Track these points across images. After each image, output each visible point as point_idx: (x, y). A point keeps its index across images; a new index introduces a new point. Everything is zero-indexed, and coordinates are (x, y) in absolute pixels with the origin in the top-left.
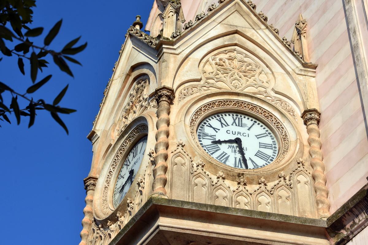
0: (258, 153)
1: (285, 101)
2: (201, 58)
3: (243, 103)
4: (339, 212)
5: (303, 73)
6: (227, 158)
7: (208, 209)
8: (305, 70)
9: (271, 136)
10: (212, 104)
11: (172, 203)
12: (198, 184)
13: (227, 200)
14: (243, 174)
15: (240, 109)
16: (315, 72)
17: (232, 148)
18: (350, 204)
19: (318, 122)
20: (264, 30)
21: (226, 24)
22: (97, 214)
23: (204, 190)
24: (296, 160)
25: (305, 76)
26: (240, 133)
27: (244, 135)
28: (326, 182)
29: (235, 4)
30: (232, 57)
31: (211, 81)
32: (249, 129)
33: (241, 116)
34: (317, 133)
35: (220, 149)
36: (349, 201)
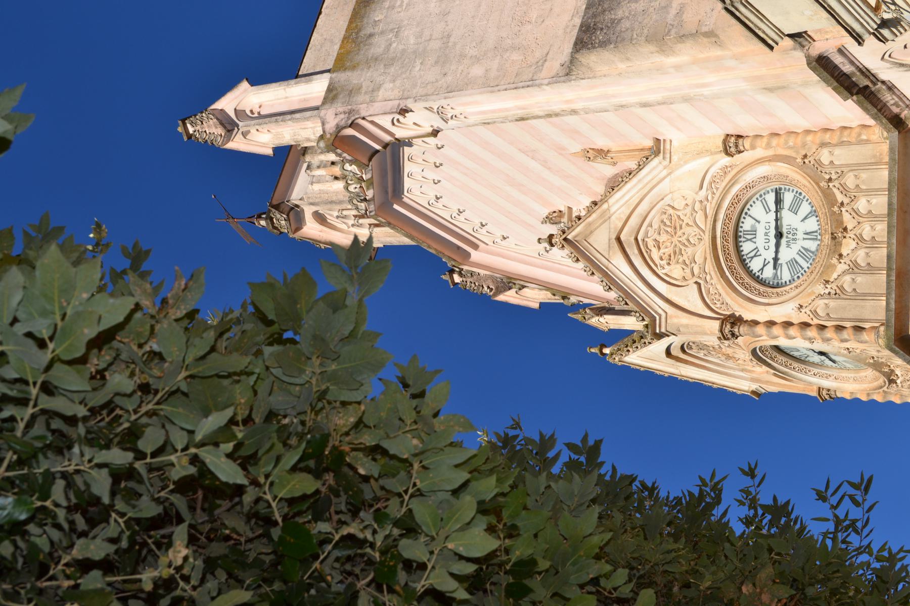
2: (665, 284)
4: (881, 122)
5: (668, 156)
6: (806, 250)
8: (664, 153)
9: (764, 194)
14: (832, 234)
15: (731, 233)
19: (739, 137)
27: (768, 227)
31: (696, 271)
32: (759, 222)
33: (741, 232)
36: (868, 114)
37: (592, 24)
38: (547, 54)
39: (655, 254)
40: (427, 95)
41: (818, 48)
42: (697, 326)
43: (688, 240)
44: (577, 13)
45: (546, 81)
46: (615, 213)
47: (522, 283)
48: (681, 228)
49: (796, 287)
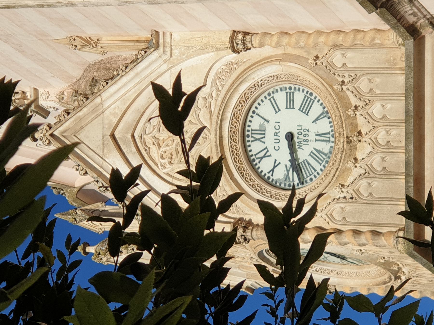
0: (304, 111)
1: (217, 73)
3: (231, 131)
4: (399, 31)
5: (168, 49)
7: (411, 185)
9: (273, 93)
10: (240, 172)
11: (410, 228)
12: (369, 191)
13: (387, 158)
14: (347, 138)
15: (239, 133)
16: (164, 32)
17: (301, 145)
18: (392, 23)
19: (246, 34)
20: (103, 99)
21: (103, 150)
22: (378, 283)
23: (375, 184)
25: (171, 46)
26: (276, 133)
27: (277, 127)
28: (341, 31)
29: (64, 136)
30: (155, 142)
32: (268, 122)
34: (265, 37)
35: (306, 160)
46: (109, 107)
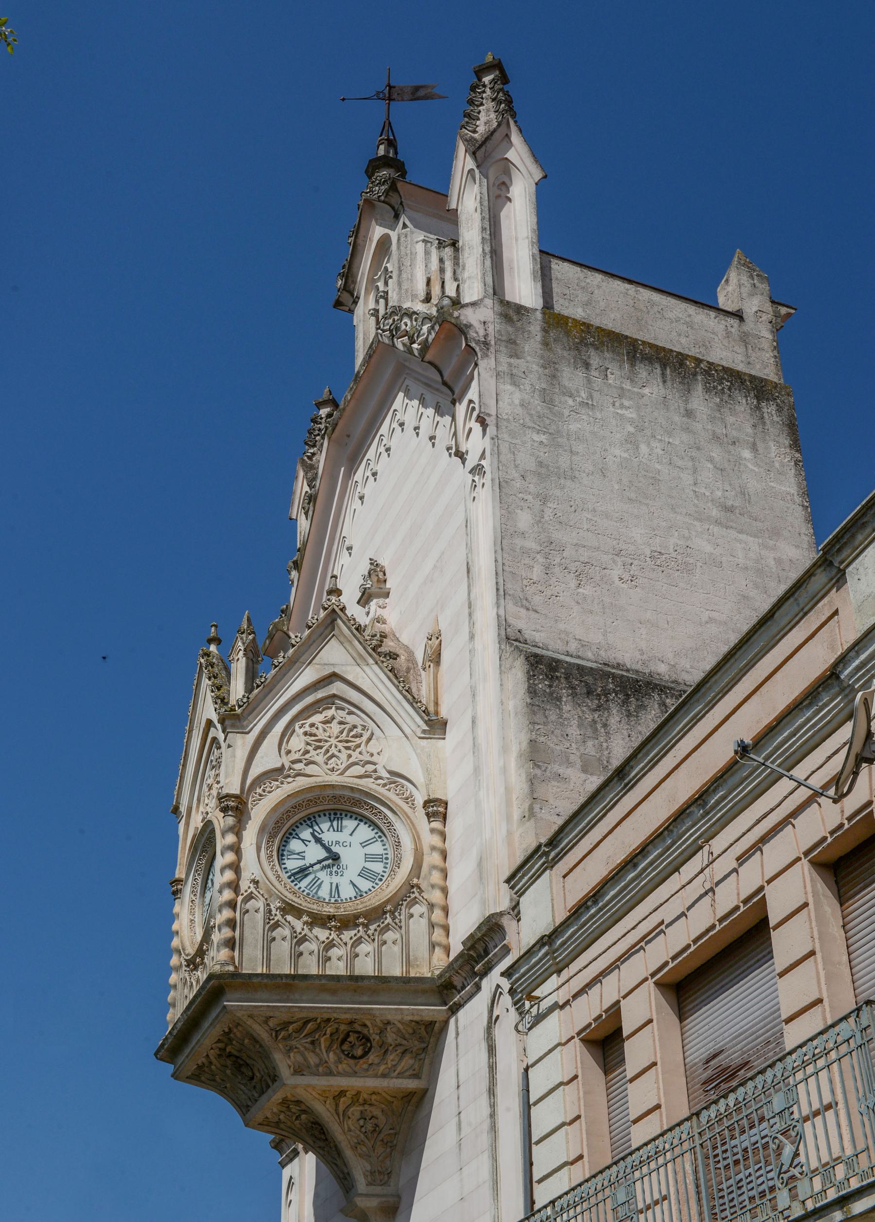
6: (320, 886)
9: (382, 841)
24: (407, 883)
31: (298, 766)
37: (558, 674)
38: (536, 611)
39: (317, 718)
40: (499, 454)
41: (508, 923)
42: (233, 767)
43: (333, 756)
44: (583, 646)
45: (502, 613)
47: (310, 513)
48: (348, 748)
49: (279, 876)
